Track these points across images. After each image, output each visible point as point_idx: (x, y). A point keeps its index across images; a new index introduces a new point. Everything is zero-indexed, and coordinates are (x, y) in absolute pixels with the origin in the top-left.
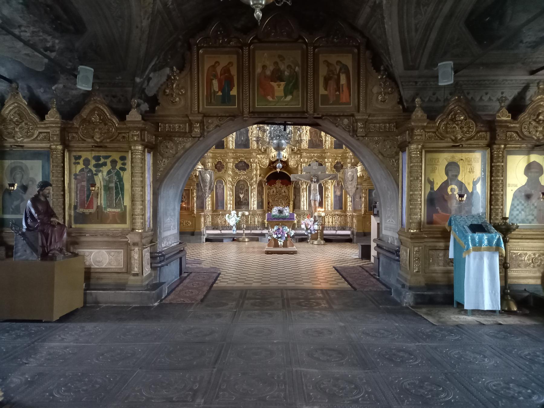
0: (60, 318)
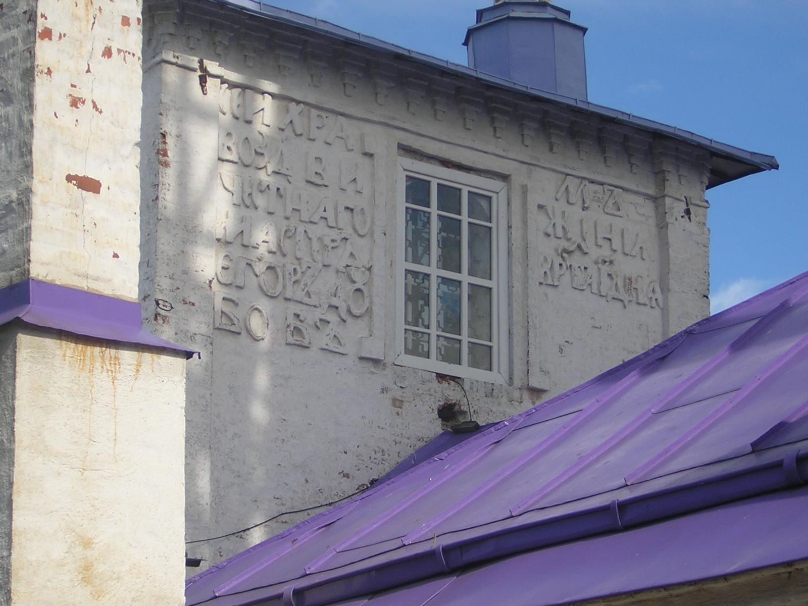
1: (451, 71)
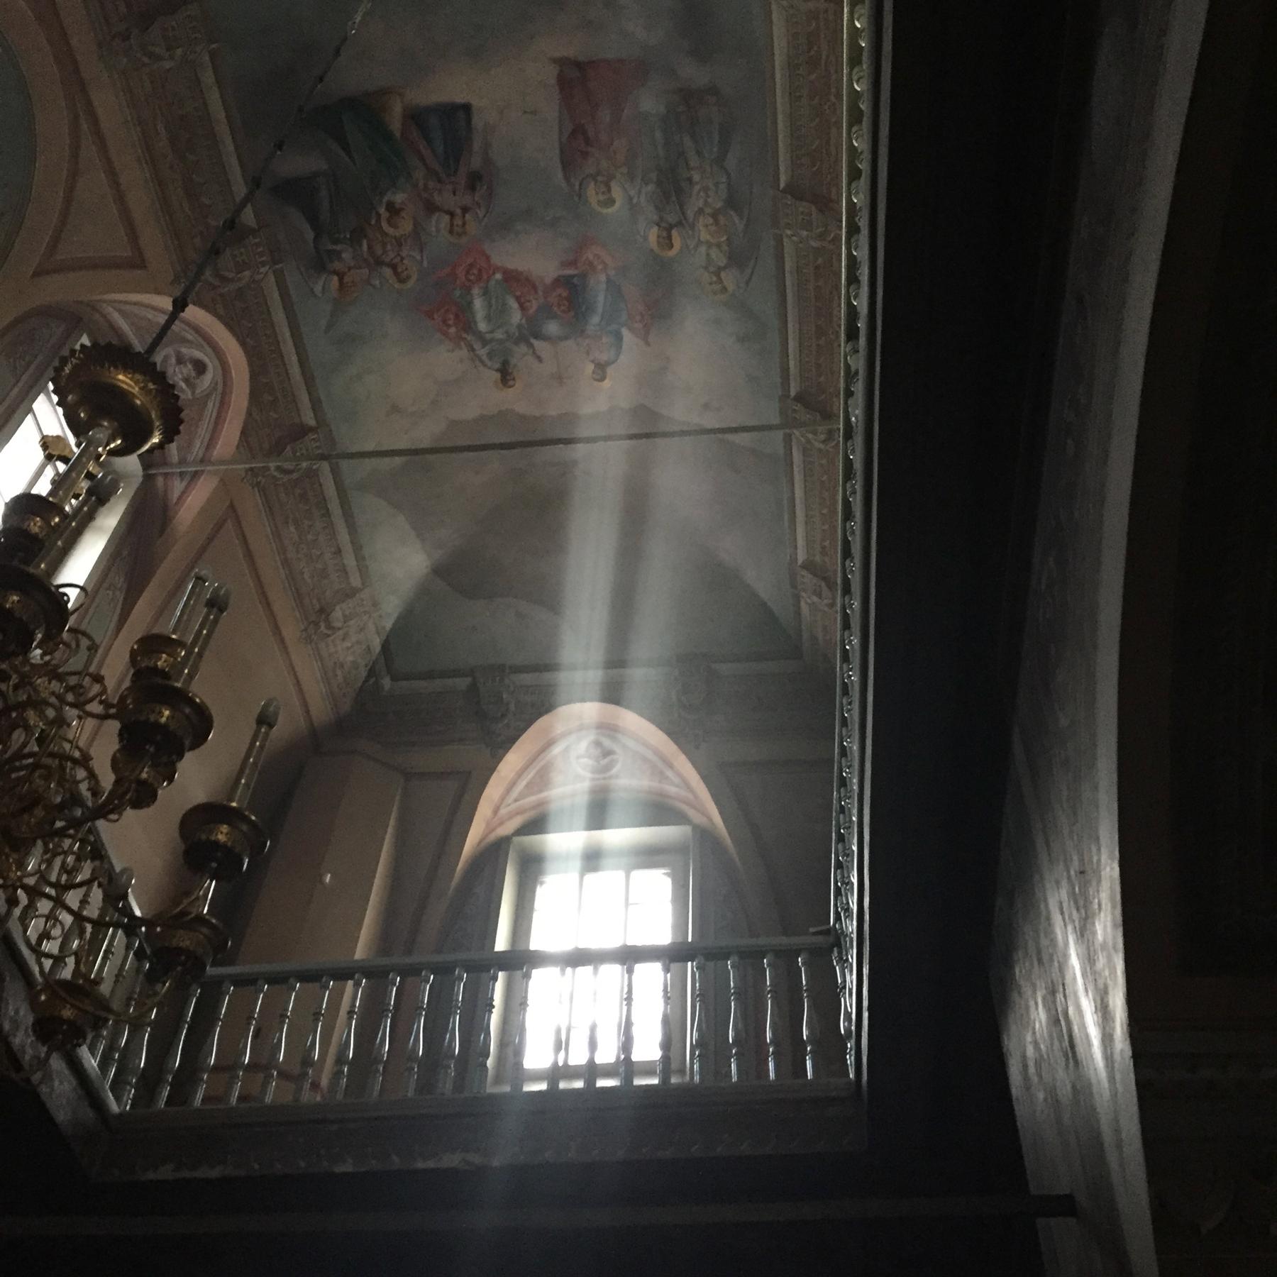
0: (849, 365)
1: (503, 1045)
